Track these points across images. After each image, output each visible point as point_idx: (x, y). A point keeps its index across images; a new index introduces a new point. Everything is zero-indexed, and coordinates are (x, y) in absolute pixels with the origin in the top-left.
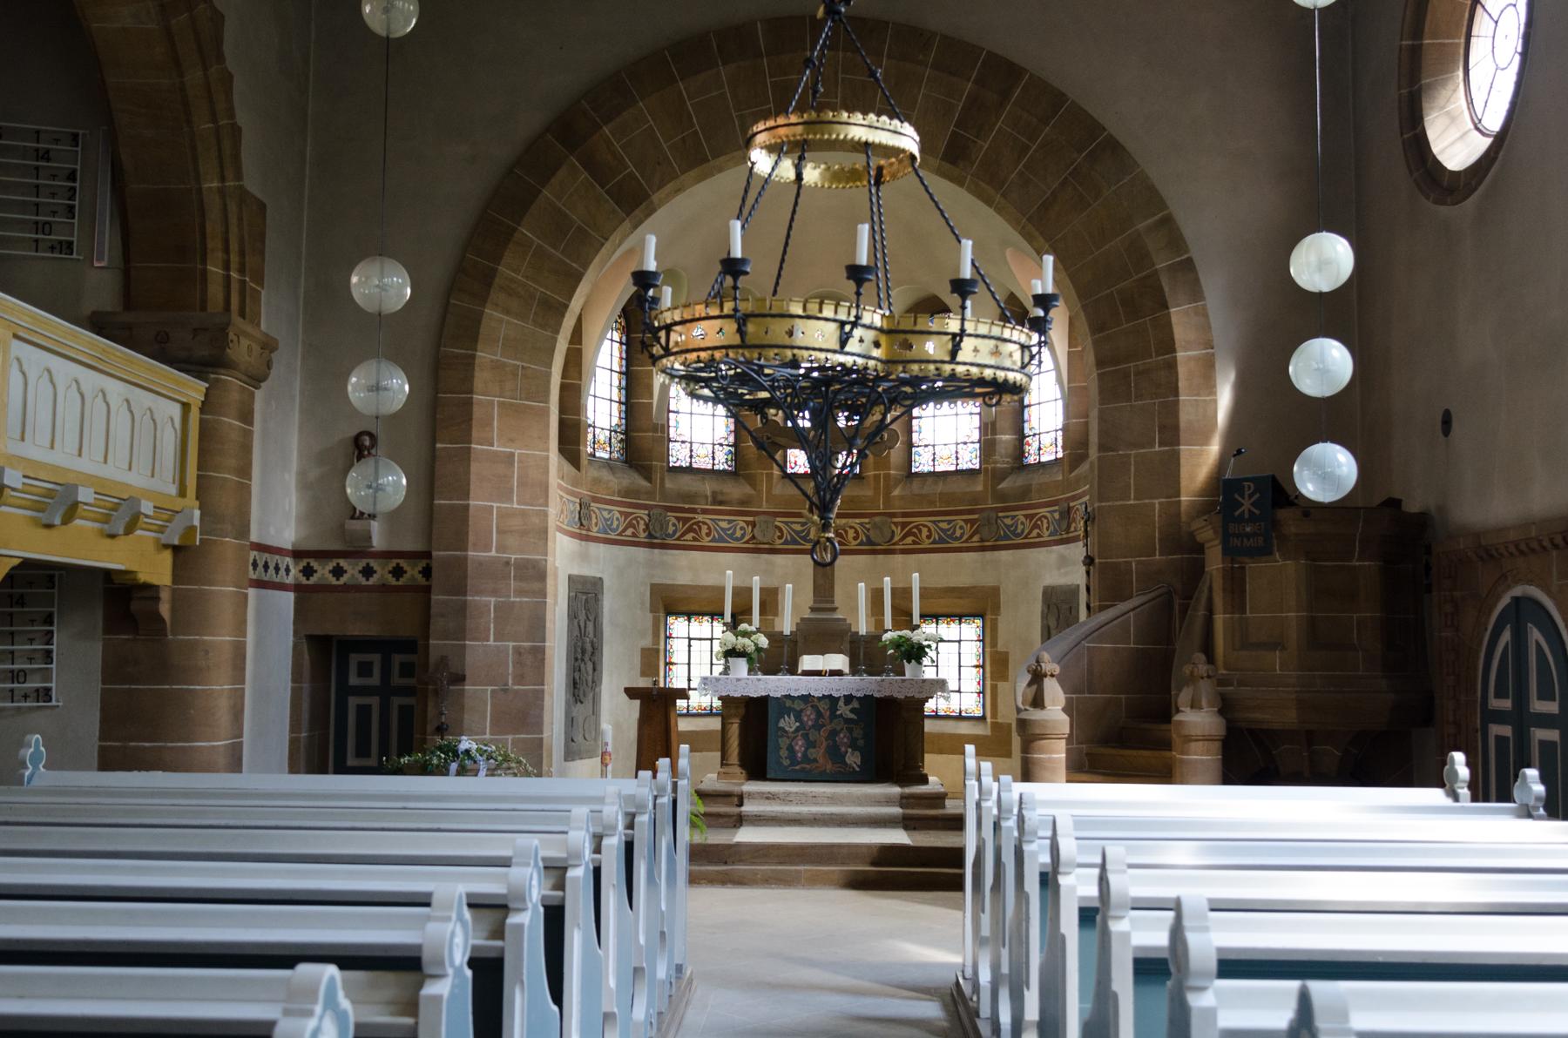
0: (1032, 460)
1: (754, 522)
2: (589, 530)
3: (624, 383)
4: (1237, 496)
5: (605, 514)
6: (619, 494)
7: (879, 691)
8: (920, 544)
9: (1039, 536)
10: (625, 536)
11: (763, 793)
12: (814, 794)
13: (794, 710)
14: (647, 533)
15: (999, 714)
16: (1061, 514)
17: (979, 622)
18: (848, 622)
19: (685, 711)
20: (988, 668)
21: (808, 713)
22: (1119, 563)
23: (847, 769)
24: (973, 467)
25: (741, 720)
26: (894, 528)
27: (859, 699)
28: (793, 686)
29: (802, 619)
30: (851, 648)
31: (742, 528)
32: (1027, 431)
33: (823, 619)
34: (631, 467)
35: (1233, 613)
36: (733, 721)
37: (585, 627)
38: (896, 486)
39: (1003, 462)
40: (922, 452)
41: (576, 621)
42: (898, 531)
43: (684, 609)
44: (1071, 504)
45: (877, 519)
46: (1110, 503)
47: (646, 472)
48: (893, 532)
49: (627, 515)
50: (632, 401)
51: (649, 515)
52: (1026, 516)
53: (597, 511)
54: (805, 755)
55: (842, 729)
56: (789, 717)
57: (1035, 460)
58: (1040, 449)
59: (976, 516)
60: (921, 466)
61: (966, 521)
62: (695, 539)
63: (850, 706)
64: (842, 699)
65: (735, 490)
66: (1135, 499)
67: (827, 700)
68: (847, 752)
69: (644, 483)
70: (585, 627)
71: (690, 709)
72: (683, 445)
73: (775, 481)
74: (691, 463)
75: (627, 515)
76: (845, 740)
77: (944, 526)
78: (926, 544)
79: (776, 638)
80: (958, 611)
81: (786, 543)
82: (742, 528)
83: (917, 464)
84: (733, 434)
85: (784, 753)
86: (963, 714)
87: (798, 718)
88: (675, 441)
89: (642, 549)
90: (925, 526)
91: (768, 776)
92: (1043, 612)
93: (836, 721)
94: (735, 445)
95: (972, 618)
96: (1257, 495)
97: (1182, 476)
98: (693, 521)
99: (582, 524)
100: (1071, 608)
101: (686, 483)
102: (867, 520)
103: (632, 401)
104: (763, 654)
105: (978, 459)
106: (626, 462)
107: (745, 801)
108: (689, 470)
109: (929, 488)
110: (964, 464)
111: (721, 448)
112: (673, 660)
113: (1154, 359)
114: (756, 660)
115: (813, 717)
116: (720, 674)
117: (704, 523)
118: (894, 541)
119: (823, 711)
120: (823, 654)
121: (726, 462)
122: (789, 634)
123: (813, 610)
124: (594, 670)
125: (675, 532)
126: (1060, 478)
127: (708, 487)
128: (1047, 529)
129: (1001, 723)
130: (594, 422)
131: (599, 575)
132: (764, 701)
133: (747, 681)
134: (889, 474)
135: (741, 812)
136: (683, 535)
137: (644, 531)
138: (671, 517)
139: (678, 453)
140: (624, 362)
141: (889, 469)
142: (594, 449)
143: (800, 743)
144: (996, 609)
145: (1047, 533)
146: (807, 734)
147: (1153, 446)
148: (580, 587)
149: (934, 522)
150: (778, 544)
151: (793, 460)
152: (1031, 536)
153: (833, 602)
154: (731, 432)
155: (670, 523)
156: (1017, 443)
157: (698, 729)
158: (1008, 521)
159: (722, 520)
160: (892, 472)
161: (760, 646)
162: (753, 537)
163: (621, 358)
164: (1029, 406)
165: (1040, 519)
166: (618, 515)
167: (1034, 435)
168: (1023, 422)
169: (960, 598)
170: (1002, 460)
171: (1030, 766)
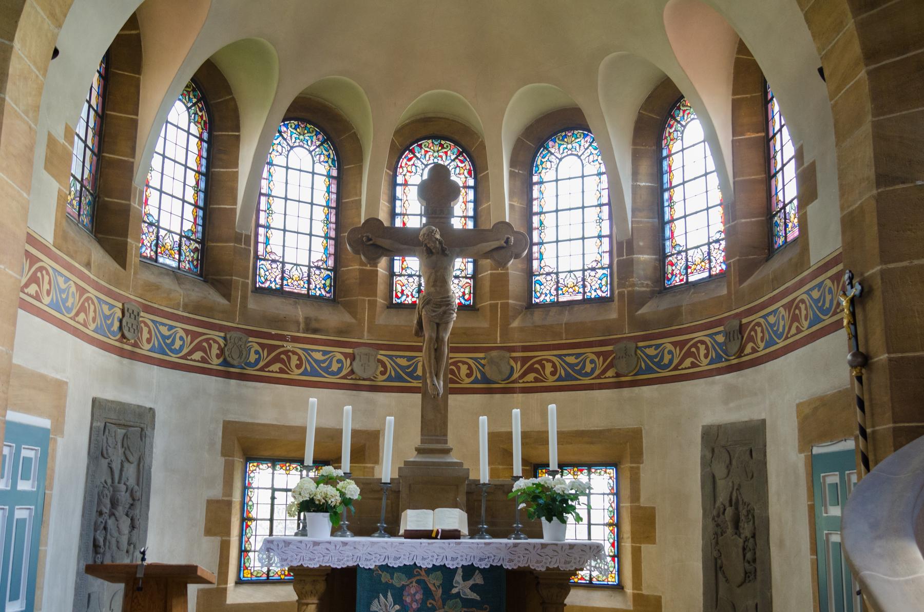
0: (677, 281)
1: (353, 354)
2: (135, 345)
3: (202, 185)
6: (186, 307)
7: (511, 561)
10: (191, 360)
13: (392, 587)
14: (221, 360)
15: (644, 585)
16: (727, 335)
17: (612, 472)
18: (465, 467)
20: (627, 527)
21: (413, 591)
24: (604, 295)
25: (319, 599)
27: (483, 571)
29: (406, 463)
30: (468, 500)
31: (339, 361)
33: (434, 464)
34: (206, 281)
36: (309, 601)
37: (121, 470)
38: (514, 318)
39: (642, 285)
40: (543, 281)
41: (104, 463)
43: (267, 454)
45: (494, 354)
47: (224, 287)
48: (512, 368)
49: (195, 335)
51: (225, 338)
52: (675, 344)
56: (386, 597)
57: (681, 280)
58: (687, 267)
59: (610, 348)
61: (598, 354)
62: (282, 371)
63: (471, 582)
64: (460, 571)
65: (333, 318)
67: (439, 573)
69: (223, 301)
70: (121, 470)
71: (271, 574)
73: (378, 309)
74: (282, 285)
78: (551, 381)
79: (370, 487)
81: (390, 379)
82: (339, 361)
84: (332, 258)
88: (265, 260)
93: (450, 602)
94: (335, 270)
98: (282, 349)
99: (123, 336)
101: (275, 306)
102: (482, 355)
104: (352, 508)
106: (201, 275)
108: (280, 292)
109: (552, 318)
111: (318, 272)
116: (296, 534)
117: (294, 353)
119: (433, 588)
121: (324, 288)
124: (133, 527)
127: (300, 312)
128: (706, 356)
129: (648, 596)
130: (158, 221)
131: (148, 405)
132: (350, 574)
133: (328, 546)
134: (508, 303)
136: (268, 365)
137: (218, 356)
142: (156, 253)
144: (637, 455)
148: (113, 416)
149: (559, 356)
150: (381, 380)
151: (399, 288)
152: (683, 366)
153: (446, 442)
155: (252, 351)
156: (657, 264)
157: (278, 600)
158: (651, 352)
161: (348, 496)
162: (352, 372)
163: (200, 156)
165: (695, 345)
166: (181, 333)
167: (679, 253)
168: (664, 239)
169: (592, 443)
170: (641, 282)
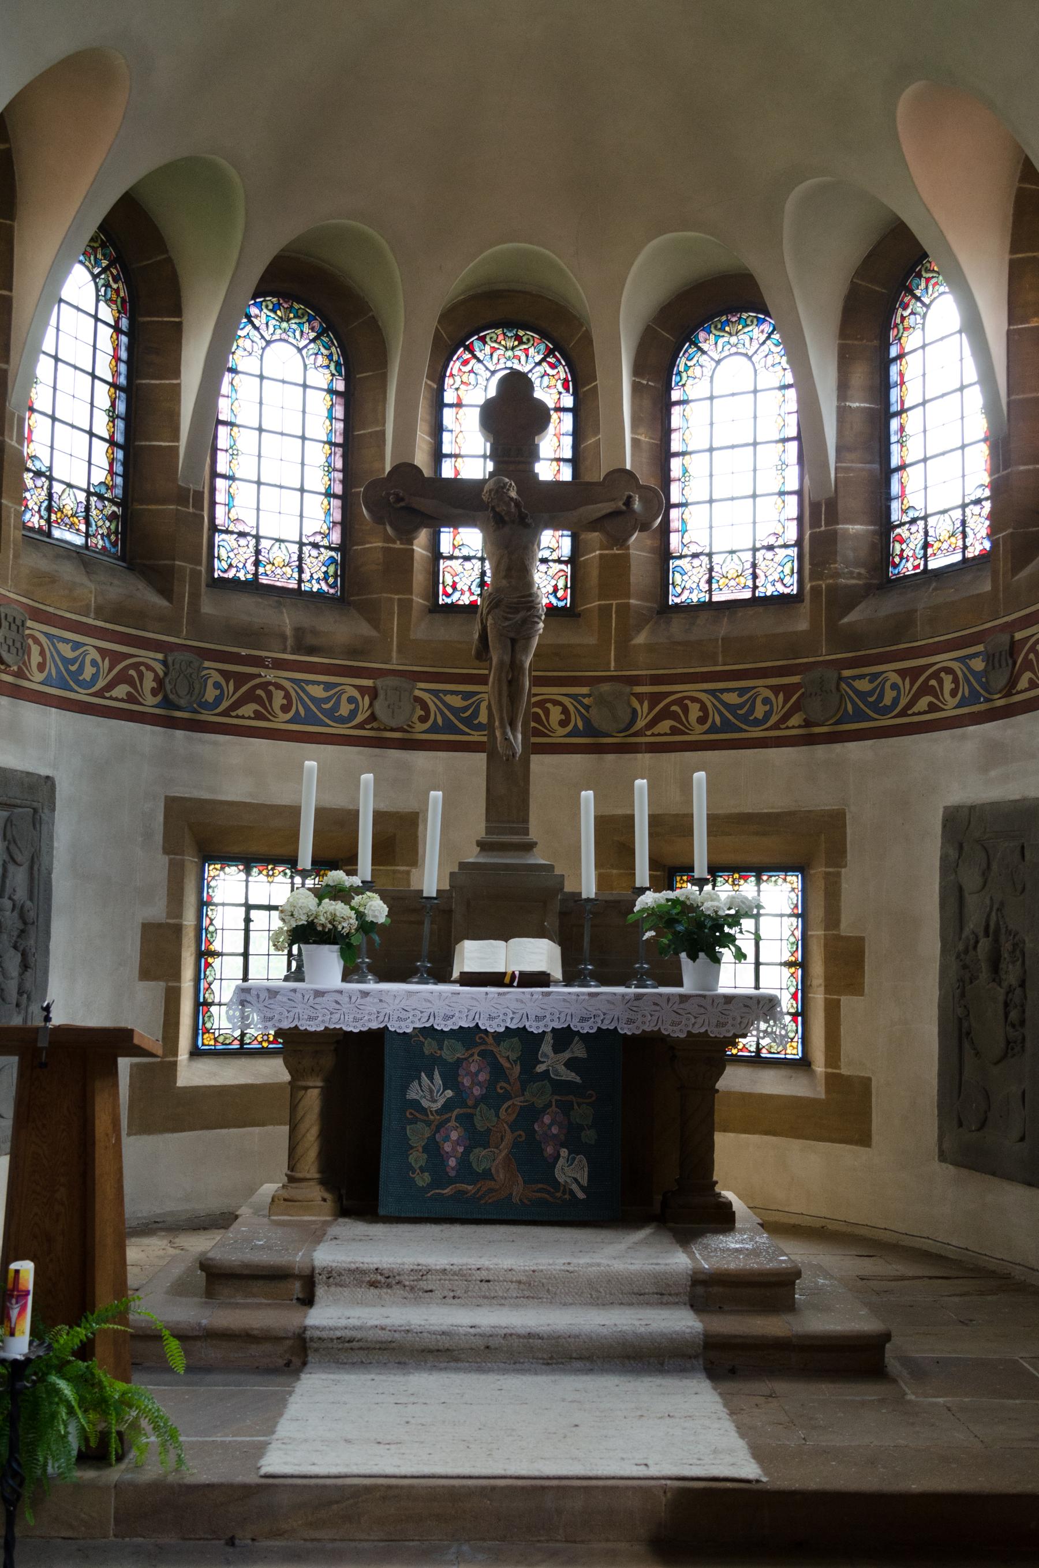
0: (908, 568)
2: (20, 674)
3: (121, 407)
5: (66, 650)
6: (100, 612)
7: (630, 1021)
8: (684, 733)
9: (932, 708)
10: (111, 698)
11: (364, 1272)
12: (484, 1275)
14: (159, 698)
16: (990, 659)
19: (236, 1045)
20: (817, 969)
21: (473, 1068)
23: (559, 1195)
24: (787, 591)
26: (636, 704)
27: (586, 1037)
28: (440, 1008)
29: (462, 865)
31: (351, 700)
32: (895, 516)
33: (507, 867)
36: (311, 1084)
38: (639, 628)
42: (643, 710)
43: (236, 849)
44: (1018, 636)
45: (605, 688)
48: (634, 712)
49: (116, 658)
50: (137, 443)
51: (165, 663)
52: (902, 673)
53: (43, 639)
54: (464, 1162)
55: (549, 1105)
56: (431, 1078)
58: (926, 545)
59: (795, 679)
60: (686, 593)
61: (776, 689)
62: (258, 716)
63: (567, 1055)
64: (549, 1038)
67: (516, 1040)
68: (558, 1157)
72: (243, 542)
73: (415, 613)
74: (256, 574)
75: (116, 658)
76: (555, 1130)
77: (732, 698)
80: (755, 859)
81: (434, 729)
83: (679, 590)
85: (417, 1158)
86: (764, 1054)
87: (451, 1080)
88: (227, 532)
89: (148, 727)
90: (694, 700)
91: (382, 1212)
92: (944, 859)
94: (342, 548)
95: (782, 875)
100: (1023, 847)
102: (585, 690)
103: (137, 443)
105: (795, 576)
107: (320, 1291)
108: (253, 586)
109: (702, 630)
110: (769, 586)
111: (314, 553)
112: (216, 946)
114: (364, 950)
115: (483, 1077)
117: (279, 687)
118: (632, 731)
119: (506, 1065)
120: (506, 940)
122: (434, 895)
123: (483, 846)
124: (25, 966)
125: (218, 700)
126: (987, 587)
127: (287, 620)
128: (954, 693)
130: (50, 468)
131: (44, 771)
133: (338, 997)
134: (628, 605)
135: (305, 1328)
137: (154, 692)
138: (212, 670)
139: (231, 555)
140: (123, 368)
141: (629, 598)
142: (48, 521)
143: (454, 1135)
144: (837, 854)
145: (952, 702)
146: (471, 1116)
149: (712, 692)
150: (420, 731)
151: (449, 580)
152: (915, 709)
154: (335, 523)
155: (210, 682)
158: (863, 685)
159: (314, 683)
160: (632, 601)
161: (369, 919)
162: (373, 717)
163: (116, 358)
164: (903, 467)
165: (936, 675)
166: (94, 654)
167: (913, 521)
168: (889, 499)
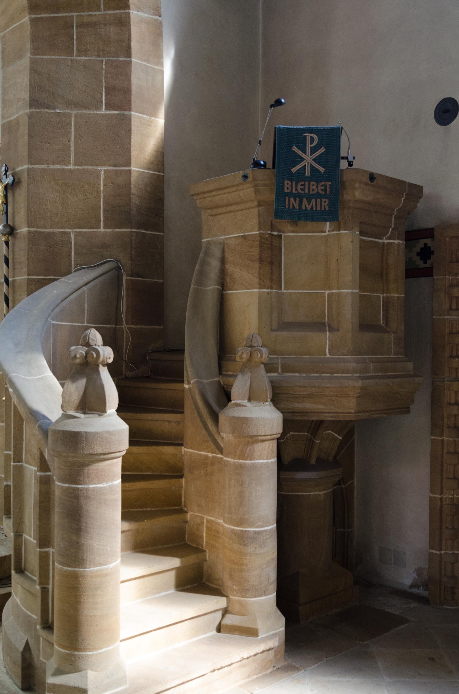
4: (295, 149)
22: (54, 233)
35: (271, 288)
46: (44, 166)
66: (75, 164)
96: (322, 150)
97: (133, 144)
113: (102, 12)
147: (99, 108)
171: (82, 500)
